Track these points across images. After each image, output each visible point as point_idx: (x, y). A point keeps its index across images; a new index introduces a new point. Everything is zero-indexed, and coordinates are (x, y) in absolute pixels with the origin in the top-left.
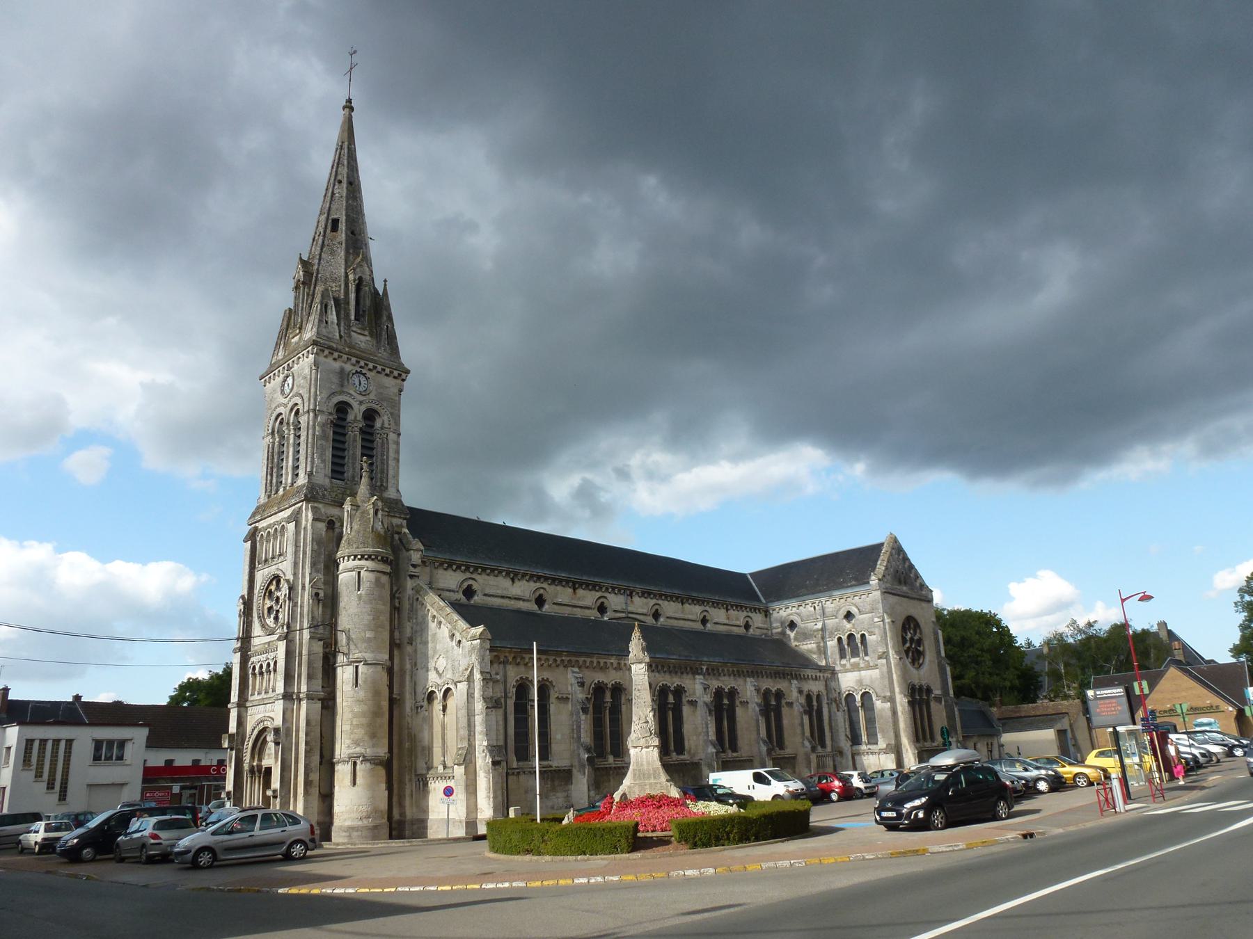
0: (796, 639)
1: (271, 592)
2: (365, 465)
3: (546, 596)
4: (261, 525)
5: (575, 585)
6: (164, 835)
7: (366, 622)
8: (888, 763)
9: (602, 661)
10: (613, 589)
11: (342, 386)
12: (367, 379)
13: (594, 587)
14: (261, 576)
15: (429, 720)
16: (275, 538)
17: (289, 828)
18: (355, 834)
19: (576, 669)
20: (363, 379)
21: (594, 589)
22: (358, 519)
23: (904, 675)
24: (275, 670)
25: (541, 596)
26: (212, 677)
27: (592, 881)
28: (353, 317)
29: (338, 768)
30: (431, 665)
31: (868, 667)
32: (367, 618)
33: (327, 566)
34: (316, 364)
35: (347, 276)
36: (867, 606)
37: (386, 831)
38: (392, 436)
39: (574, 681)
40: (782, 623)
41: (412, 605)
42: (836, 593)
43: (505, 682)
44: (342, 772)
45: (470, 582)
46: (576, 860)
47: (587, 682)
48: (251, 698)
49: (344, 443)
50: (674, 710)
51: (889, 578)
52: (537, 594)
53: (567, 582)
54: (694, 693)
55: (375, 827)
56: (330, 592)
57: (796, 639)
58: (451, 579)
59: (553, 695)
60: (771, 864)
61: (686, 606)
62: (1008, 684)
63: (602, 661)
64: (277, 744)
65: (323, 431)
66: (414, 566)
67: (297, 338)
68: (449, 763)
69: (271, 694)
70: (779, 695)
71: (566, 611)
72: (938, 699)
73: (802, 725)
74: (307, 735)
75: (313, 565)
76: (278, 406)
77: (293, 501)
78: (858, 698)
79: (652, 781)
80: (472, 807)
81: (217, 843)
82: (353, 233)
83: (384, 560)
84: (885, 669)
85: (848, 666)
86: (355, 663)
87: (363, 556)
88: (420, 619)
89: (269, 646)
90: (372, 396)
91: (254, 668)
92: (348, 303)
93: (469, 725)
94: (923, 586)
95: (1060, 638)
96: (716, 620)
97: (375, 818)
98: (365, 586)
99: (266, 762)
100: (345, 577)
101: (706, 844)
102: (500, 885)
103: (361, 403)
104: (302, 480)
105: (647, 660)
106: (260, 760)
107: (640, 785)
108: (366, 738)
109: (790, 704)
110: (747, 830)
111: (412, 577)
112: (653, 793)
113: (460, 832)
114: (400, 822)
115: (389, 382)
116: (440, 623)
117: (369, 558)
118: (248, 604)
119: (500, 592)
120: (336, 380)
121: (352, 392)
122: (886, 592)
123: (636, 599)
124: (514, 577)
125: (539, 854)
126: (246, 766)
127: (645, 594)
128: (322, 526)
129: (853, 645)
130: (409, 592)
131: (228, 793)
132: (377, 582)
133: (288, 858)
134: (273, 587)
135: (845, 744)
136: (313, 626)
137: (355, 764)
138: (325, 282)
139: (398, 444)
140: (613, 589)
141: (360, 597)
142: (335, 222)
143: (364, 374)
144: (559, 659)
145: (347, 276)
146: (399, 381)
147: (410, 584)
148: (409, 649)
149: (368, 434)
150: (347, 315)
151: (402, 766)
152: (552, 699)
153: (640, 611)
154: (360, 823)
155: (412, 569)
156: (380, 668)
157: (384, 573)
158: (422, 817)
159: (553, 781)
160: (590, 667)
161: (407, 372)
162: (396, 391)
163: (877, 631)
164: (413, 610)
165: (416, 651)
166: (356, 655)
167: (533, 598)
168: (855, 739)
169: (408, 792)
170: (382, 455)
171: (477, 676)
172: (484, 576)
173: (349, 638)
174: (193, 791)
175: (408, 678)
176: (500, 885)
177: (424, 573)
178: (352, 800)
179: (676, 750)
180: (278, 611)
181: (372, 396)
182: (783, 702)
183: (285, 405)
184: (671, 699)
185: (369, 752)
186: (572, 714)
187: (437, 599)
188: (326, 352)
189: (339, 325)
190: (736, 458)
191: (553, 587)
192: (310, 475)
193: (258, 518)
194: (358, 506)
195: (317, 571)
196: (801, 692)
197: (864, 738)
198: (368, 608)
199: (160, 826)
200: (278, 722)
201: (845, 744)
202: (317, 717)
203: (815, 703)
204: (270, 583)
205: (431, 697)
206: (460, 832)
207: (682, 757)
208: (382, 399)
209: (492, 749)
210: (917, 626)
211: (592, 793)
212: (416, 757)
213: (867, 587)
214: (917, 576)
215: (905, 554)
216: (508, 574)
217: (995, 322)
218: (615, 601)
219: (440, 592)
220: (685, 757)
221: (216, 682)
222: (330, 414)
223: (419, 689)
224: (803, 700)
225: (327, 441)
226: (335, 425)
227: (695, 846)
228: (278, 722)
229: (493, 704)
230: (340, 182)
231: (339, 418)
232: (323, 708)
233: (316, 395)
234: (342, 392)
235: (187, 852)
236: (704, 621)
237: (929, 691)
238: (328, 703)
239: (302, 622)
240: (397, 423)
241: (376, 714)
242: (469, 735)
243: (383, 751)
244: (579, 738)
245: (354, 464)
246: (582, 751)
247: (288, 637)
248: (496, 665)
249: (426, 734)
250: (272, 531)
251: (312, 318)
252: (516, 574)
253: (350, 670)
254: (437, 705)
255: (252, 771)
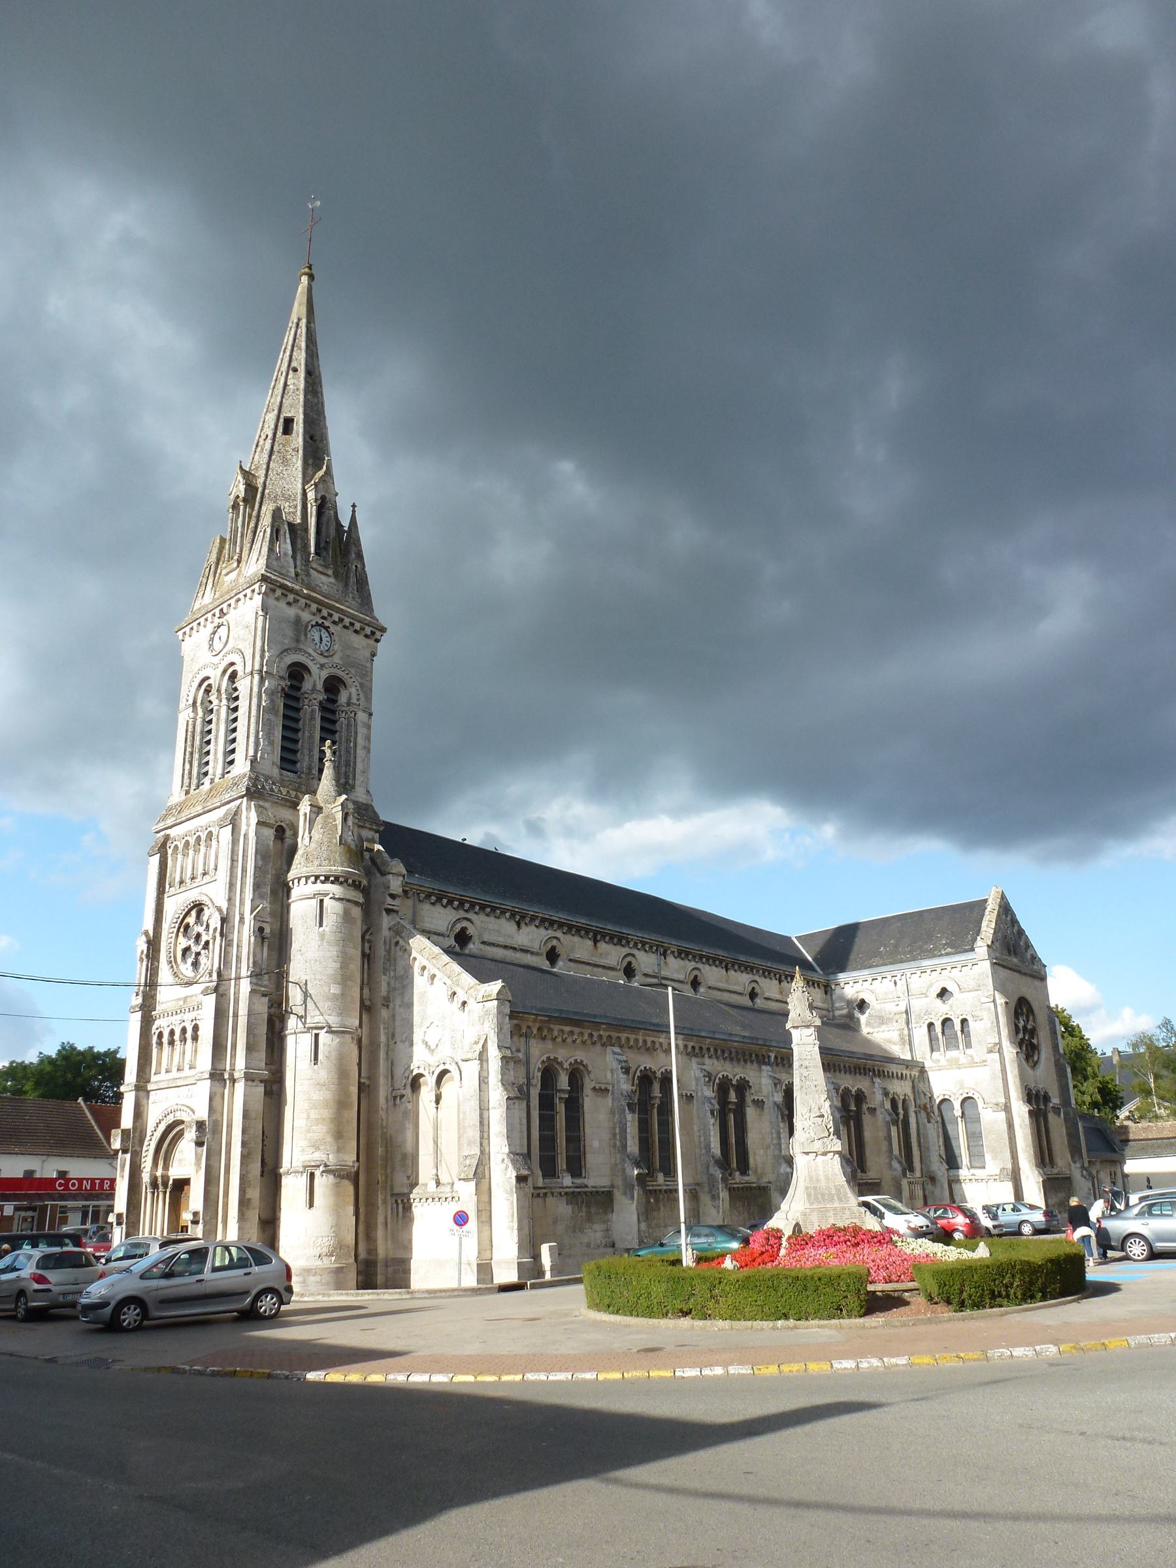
0: (868, 1024)
1: (187, 927)
2: (328, 753)
3: (559, 950)
4: (173, 832)
5: (597, 937)
6: (54, 1276)
7: (330, 971)
8: (1003, 1193)
9: (649, 1039)
10: (644, 944)
11: (298, 641)
12: (331, 634)
13: (618, 940)
14: (174, 906)
15: (413, 1117)
16: (197, 851)
17: (256, 1269)
18: (312, 1279)
19: (617, 1049)
20: (325, 635)
21: (619, 943)
22: (320, 830)
23: (1022, 1076)
24: (195, 1038)
25: (553, 948)
26: (42, 1061)
27: (864, 1365)
28: (312, 550)
29: (285, 1181)
30: (417, 1037)
31: (973, 1064)
32: (332, 966)
33: (275, 890)
34: (265, 608)
35: (304, 494)
36: (970, 982)
37: (352, 1276)
38: (361, 716)
39: (615, 1065)
40: (849, 1003)
41: (389, 951)
42: (926, 963)
43: (528, 1063)
44: (292, 1189)
45: (465, 924)
46: (774, 1328)
47: (633, 1067)
48: (153, 1078)
49: (297, 720)
50: (735, 1112)
51: (997, 944)
52: (549, 946)
53: (587, 932)
54: (760, 1091)
55: (339, 1271)
56: (277, 926)
57: (868, 1024)
58: (442, 917)
59: (588, 1084)
60: (1142, 1339)
61: (732, 972)
62: (1087, 1099)
63: (649, 1039)
64: (199, 1144)
65: (272, 701)
66: (393, 896)
67: (233, 575)
68: (444, 1179)
69: (187, 1072)
70: (860, 1097)
71: (587, 974)
72: (1056, 1111)
73: (889, 1138)
74: (244, 1132)
75: (257, 886)
76: (205, 667)
77: (227, 797)
78: (957, 1105)
79: (837, 1205)
80: (486, 1245)
81: (149, 1291)
82: (311, 438)
83: (356, 885)
84: (998, 1066)
85: (943, 1062)
86: (315, 1031)
87: (327, 878)
88: (400, 971)
89: (185, 1001)
90: (336, 659)
91: (160, 1035)
92: (306, 530)
93: (481, 1123)
94: (1034, 958)
95: (1146, 1040)
96: (767, 995)
97: (338, 1257)
98: (330, 920)
99: (176, 1172)
100: (301, 910)
101: (978, 1305)
102: (707, 1372)
103: (322, 666)
104: (242, 767)
105: (818, 1022)
106: (166, 1167)
107: (819, 1210)
108: (329, 1139)
109: (873, 1111)
110: (1031, 1283)
111: (389, 911)
112: (840, 1224)
113: (470, 1281)
114: (375, 1263)
115: (359, 641)
116: (433, 977)
117: (337, 880)
118: (153, 944)
119: (501, 940)
120: (290, 632)
121: (311, 651)
122: (997, 964)
123: (671, 960)
124: (520, 920)
125: (705, 1317)
126: (146, 1177)
127: (683, 954)
128: (270, 833)
129: (949, 1032)
130: (385, 933)
131: (119, 1216)
132: (346, 916)
133: (251, 1316)
134: (191, 920)
135: (939, 1168)
136: (256, 975)
137: (312, 1175)
138: (275, 499)
139: (369, 727)
140: (644, 944)
141: (322, 936)
142: (289, 422)
143: (327, 628)
144: (595, 1034)
145: (304, 494)
146: (371, 642)
147: (386, 921)
148: (384, 1013)
149: (329, 710)
150: (306, 546)
151: (378, 1179)
152: (587, 1090)
153: (675, 976)
154: (319, 1263)
155: (389, 900)
156: (348, 1037)
157: (356, 903)
158: (400, 1255)
159: (588, 1206)
160: (635, 1047)
161: (383, 630)
162: (368, 655)
163: (985, 1014)
164: (390, 959)
165: (394, 1016)
166: (314, 1018)
167: (544, 950)
168: (952, 1162)
169: (380, 1220)
170: (348, 741)
171: (494, 1054)
172: (482, 917)
173: (306, 994)
174: (30, 1213)
175: (382, 1055)
176: (707, 1372)
177: (405, 906)
178: (308, 1233)
179: (739, 1169)
180: (198, 954)
181: (336, 659)
182: (865, 1107)
183: (216, 667)
184: (733, 1097)
185: (332, 1160)
186: (612, 1112)
187: (426, 942)
188: (279, 592)
189: (294, 557)
190: (679, 812)
191: (569, 937)
192: (254, 761)
193: (170, 822)
194: (320, 809)
195: (262, 897)
196: (886, 1094)
197: (965, 1159)
198: (333, 951)
199: (47, 1262)
200: (203, 1114)
201: (939, 1168)
202: (258, 1105)
203: (901, 1111)
204: (188, 913)
205: (415, 1083)
206: (470, 1281)
207: (746, 1178)
208: (349, 663)
209: (520, 1156)
210: (1031, 1010)
211: (643, 1226)
212: (393, 1169)
213: (970, 955)
214: (1028, 945)
215: (1013, 915)
216: (513, 916)
217: (985, 658)
218: (645, 961)
219: (428, 934)
220: (751, 1178)
221: (48, 1068)
222: (282, 678)
223: (399, 1071)
224: (888, 1106)
225: (276, 714)
226: (287, 696)
227: (962, 1305)
228: (203, 1114)
229: (518, 1094)
230: (295, 370)
231: (292, 687)
232: (266, 1093)
233: (263, 651)
234: (297, 650)
235: (103, 1305)
236: (753, 995)
237: (1046, 1098)
238: (272, 1087)
239: (238, 968)
240: (368, 699)
241: (341, 1104)
242: (482, 1138)
243: (350, 1158)
244: (624, 1146)
245: (310, 750)
246: (628, 1165)
247: (219, 991)
248: (515, 1039)
249: (409, 1135)
250: (192, 841)
251: (257, 546)
252: (523, 917)
253: (306, 1040)
254: (426, 1093)
255: (154, 1184)
